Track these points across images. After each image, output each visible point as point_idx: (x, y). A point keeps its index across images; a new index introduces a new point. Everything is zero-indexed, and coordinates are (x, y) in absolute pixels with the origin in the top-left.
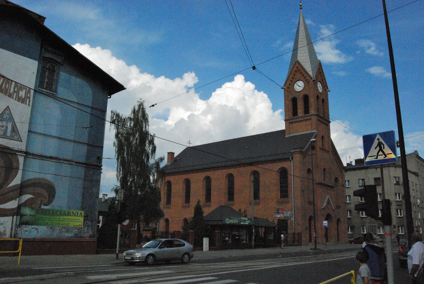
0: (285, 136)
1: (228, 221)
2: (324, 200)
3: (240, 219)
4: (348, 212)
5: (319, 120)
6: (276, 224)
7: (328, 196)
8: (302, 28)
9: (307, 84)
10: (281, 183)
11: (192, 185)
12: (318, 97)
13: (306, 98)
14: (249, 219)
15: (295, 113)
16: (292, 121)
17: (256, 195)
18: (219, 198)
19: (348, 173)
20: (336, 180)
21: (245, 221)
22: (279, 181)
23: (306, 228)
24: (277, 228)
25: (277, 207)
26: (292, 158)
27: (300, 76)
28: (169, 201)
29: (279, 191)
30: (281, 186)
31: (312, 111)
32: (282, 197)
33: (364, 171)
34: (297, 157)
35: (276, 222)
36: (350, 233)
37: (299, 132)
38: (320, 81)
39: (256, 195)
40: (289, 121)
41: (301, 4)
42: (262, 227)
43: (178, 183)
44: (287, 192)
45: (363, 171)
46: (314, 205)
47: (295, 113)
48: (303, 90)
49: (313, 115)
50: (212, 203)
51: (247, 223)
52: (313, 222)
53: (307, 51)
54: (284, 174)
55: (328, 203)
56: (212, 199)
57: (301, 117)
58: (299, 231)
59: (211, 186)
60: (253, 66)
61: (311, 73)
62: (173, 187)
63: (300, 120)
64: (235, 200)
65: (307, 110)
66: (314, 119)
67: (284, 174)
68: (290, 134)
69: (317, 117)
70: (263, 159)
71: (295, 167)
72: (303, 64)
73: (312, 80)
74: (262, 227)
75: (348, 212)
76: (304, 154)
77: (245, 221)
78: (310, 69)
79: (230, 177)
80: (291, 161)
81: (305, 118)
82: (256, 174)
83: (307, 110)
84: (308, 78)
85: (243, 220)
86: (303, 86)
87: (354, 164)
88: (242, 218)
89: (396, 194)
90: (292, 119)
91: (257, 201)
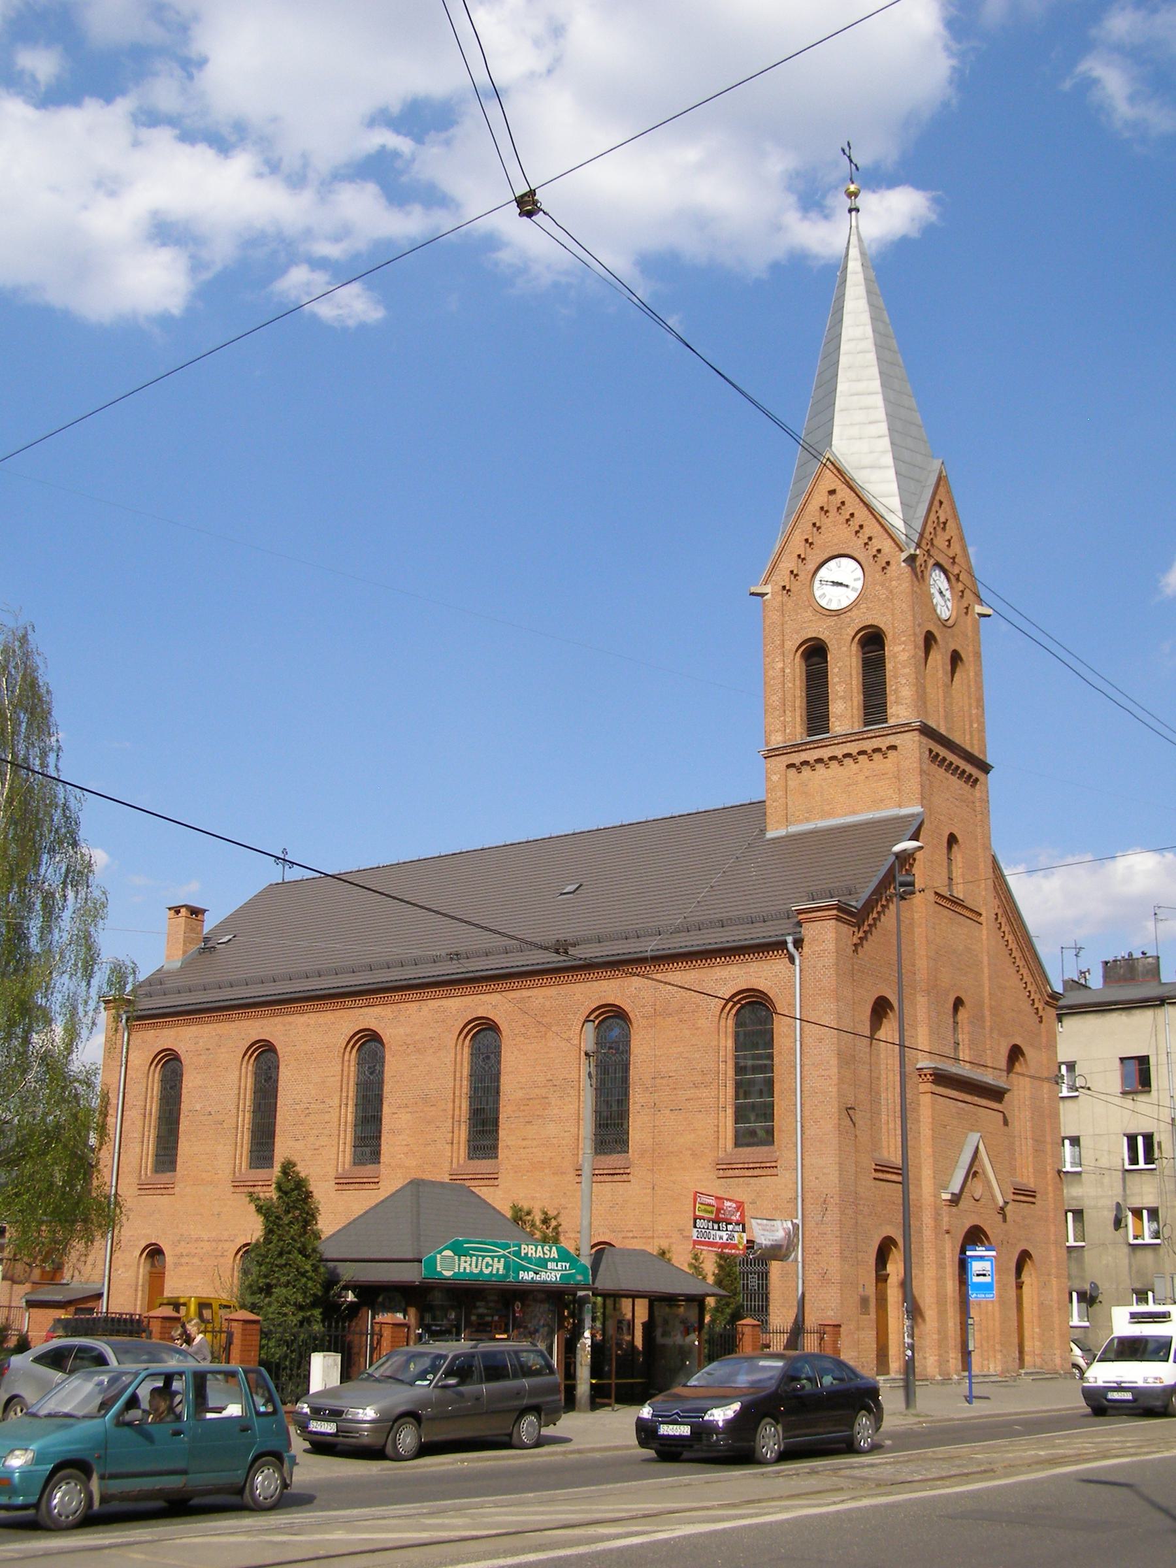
0: (763, 831)
1: (451, 1266)
2: (947, 1153)
3: (517, 1254)
4: (1070, 1215)
5: (934, 757)
6: (711, 1280)
7: (974, 1138)
8: (854, 239)
9: (879, 576)
10: (739, 1070)
11: (286, 1075)
12: (929, 640)
13: (872, 641)
14: (564, 1256)
15: (817, 717)
16: (804, 756)
17: (611, 1130)
18: (423, 1136)
19: (1072, 1025)
20: (1015, 1053)
21: (543, 1263)
22: (731, 1064)
23: (864, 1301)
24: (711, 1302)
25: (717, 1187)
26: (798, 943)
27: (846, 533)
28: (166, 1154)
29: (730, 1111)
30: (738, 1085)
31: (900, 710)
32: (743, 1139)
33: (1149, 1014)
34: (825, 937)
35: (710, 1267)
36: (1075, 1321)
37: (830, 814)
38: (938, 565)
39: (611, 1130)
40: (787, 760)
41: (852, 188)
42: (634, 1296)
43: (214, 1062)
44: (767, 1112)
45: (1144, 1018)
46: (905, 1184)
47: (817, 717)
48: (855, 604)
49: (903, 728)
50: (383, 1169)
51: (552, 1275)
52: (895, 1269)
53: (881, 414)
54: (754, 1014)
55: (973, 1173)
56: (384, 1148)
57: (849, 738)
58: (831, 1317)
59: (381, 1083)
60: (522, 189)
61: (896, 521)
62: (191, 1082)
63: (839, 751)
64: (502, 1153)
65: (874, 704)
66: (911, 743)
67: (754, 1014)
68: (787, 821)
69: (925, 740)
70: (650, 946)
71: (809, 984)
72: (860, 477)
73: (904, 556)
74: (634, 1296)
75: (1070, 1215)
76: (858, 917)
77: (543, 1263)
78: (895, 502)
79: (484, 1035)
80: (792, 960)
81: (868, 745)
82: (612, 1020)
83: (874, 704)
84: (887, 546)
85: (526, 1257)
86: (859, 585)
87: (1096, 981)
88: (529, 1250)
89: (1132, 1139)
90: (797, 748)
91: (613, 1160)
